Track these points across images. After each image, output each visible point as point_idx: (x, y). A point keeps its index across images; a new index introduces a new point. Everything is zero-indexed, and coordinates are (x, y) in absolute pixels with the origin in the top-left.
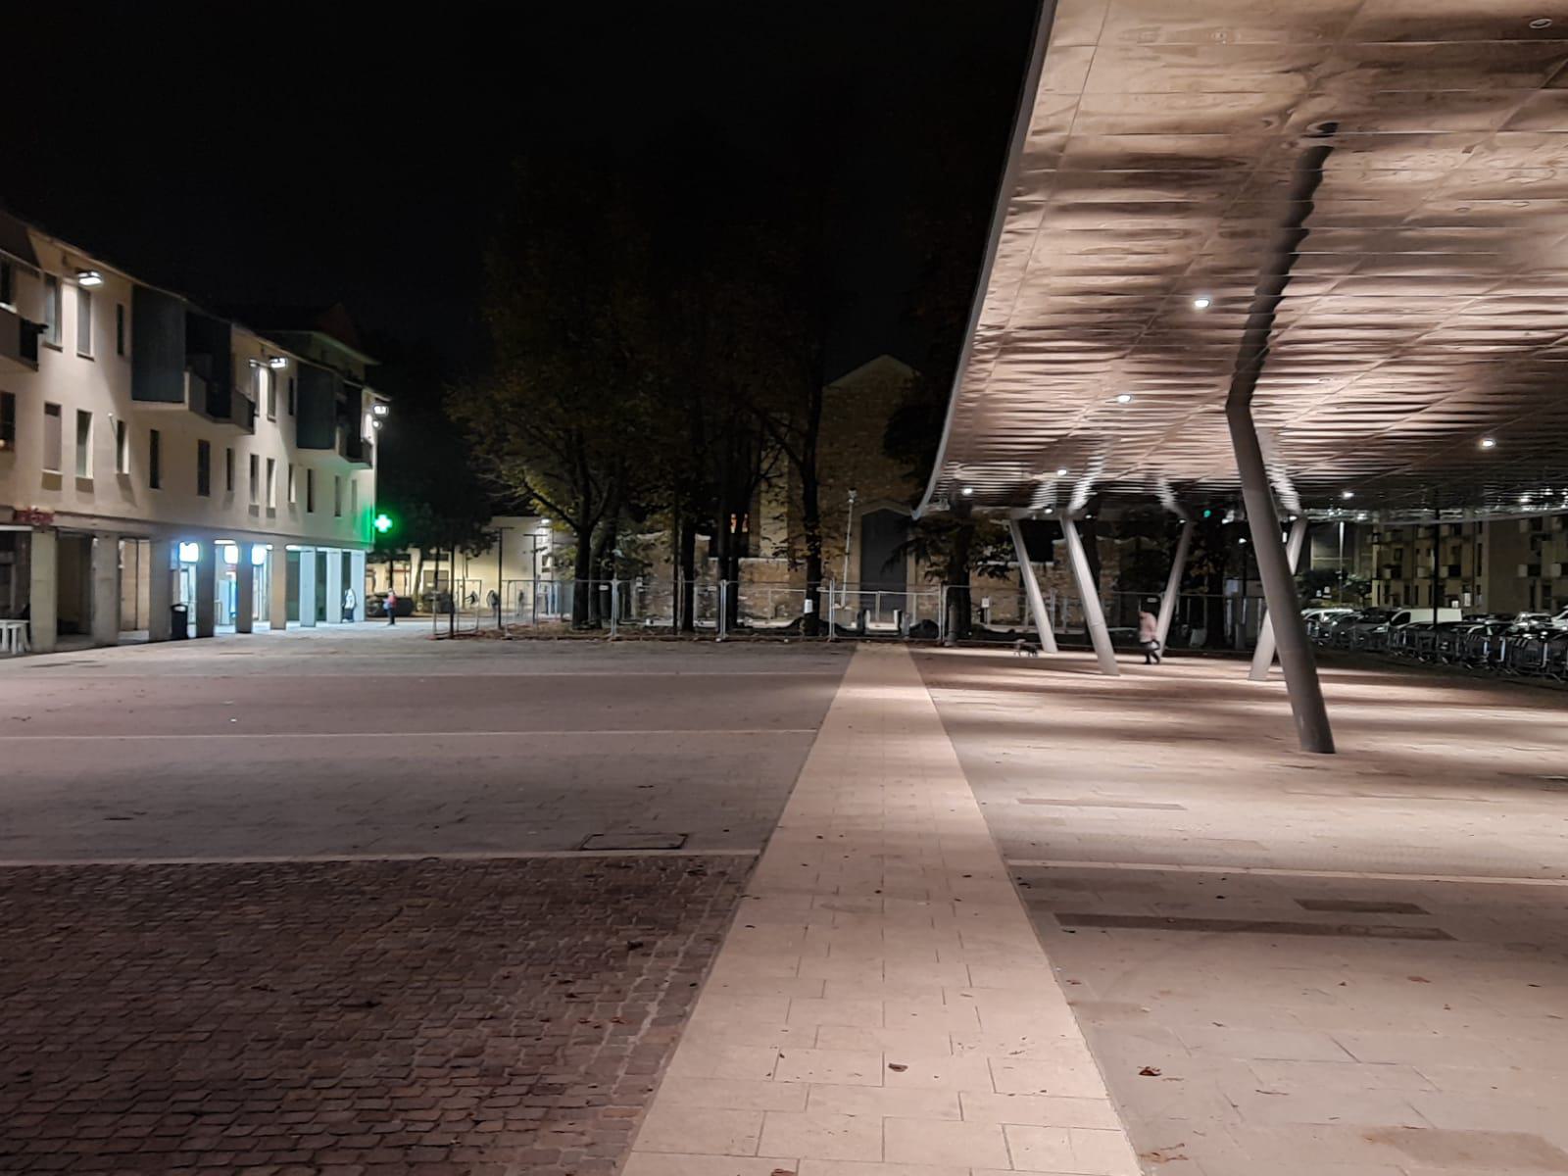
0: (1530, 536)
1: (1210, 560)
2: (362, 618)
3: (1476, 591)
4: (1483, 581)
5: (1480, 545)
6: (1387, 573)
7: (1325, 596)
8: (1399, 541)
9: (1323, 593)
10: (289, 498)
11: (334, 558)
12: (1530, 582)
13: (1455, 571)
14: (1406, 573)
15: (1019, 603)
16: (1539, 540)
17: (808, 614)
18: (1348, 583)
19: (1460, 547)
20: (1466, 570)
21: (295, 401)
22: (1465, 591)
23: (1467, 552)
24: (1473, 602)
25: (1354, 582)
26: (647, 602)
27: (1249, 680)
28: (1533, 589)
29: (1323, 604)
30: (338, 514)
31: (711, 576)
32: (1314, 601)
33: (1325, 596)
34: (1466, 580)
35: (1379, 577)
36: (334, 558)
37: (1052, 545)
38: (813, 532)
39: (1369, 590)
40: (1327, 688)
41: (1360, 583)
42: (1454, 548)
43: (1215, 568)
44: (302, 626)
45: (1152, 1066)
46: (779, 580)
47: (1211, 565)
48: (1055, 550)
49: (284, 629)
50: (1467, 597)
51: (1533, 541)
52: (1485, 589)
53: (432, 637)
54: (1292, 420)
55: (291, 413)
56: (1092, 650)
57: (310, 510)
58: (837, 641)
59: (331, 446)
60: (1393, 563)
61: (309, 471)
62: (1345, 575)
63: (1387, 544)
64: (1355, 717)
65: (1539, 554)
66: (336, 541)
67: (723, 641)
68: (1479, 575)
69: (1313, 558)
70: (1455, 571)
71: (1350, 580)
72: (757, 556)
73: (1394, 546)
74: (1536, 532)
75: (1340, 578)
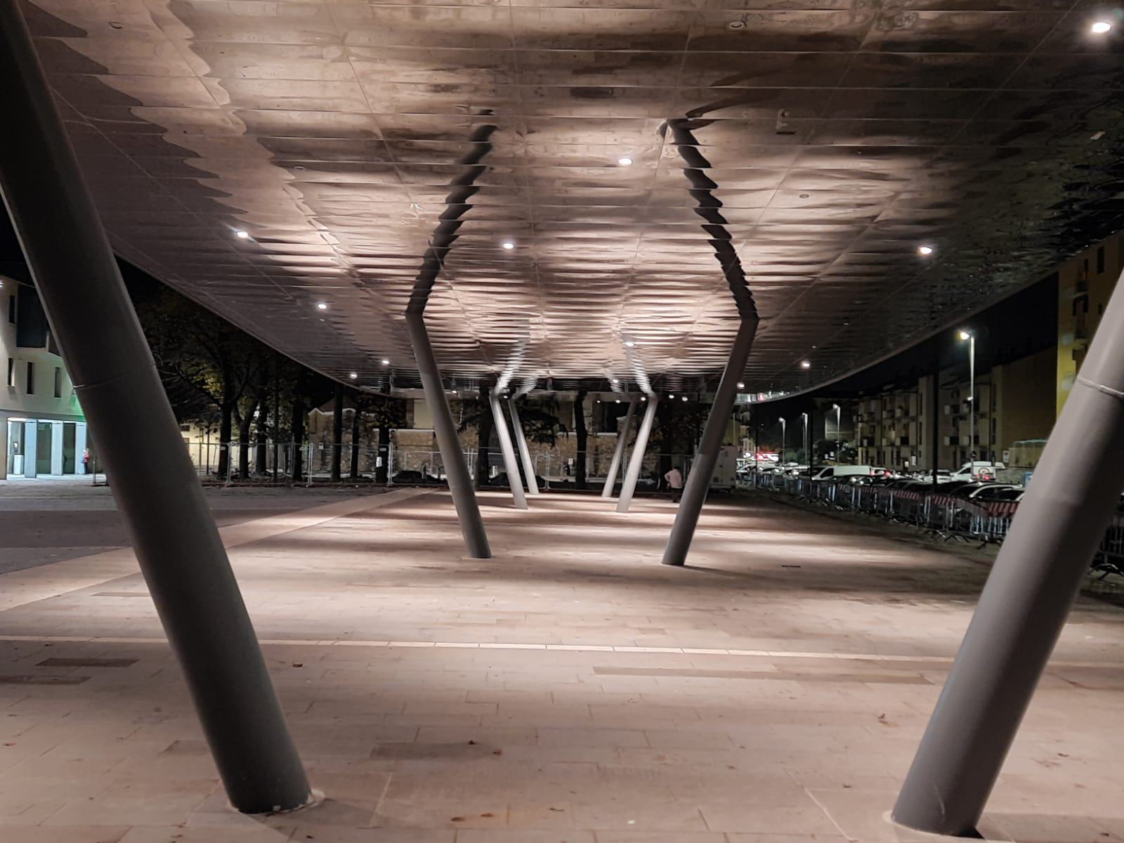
0: (951, 417)
1: (661, 430)
2: (83, 472)
3: (919, 455)
4: (922, 448)
5: (921, 423)
6: (865, 442)
7: (831, 459)
8: (873, 420)
9: (829, 456)
10: (10, 382)
11: (57, 429)
12: (952, 449)
13: (905, 441)
14: (877, 443)
15: (595, 462)
16: (958, 419)
17: (380, 468)
18: (844, 449)
19: (908, 424)
20: (912, 441)
21: (16, 310)
22: (912, 455)
23: (912, 426)
24: (917, 463)
25: (846, 448)
26: (327, 460)
27: (617, 511)
28: (955, 453)
29: (830, 464)
30: (57, 395)
31: (375, 442)
32: (824, 461)
33: (831, 459)
34: (912, 447)
35: (862, 445)
36: (57, 429)
37: (617, 421)
38: (379, 408)
39: (857, 454)
40: (485, 512)
41: (851, 449)
42: (905, 425)
43: (664, 436)
44: (26, 477)
45: (310, 835)
46: (425, 444)
47: (661, 433)
48: (618, 424)
49: (5, 479)
50: (914, 458)
51: (954, 420)
52: (924, 454)
53: (92, 484)
54: (319, 306)
55: (11, 320)
56: (509, 490)
57: (30, 391)
58: (393, 486)
59: (44, 346)
60: (870, 435)
61: (30, 365)
62: (841, 446)
63: (867, 422)
64: (608, 536)
65: (958, 430)
66: (55, 415)
67: (310, 487)
68: (921, 444)
69: (826, 432)
70: (905, 441)
71: (845, 447)
72: (412, 428)
73: (871, 424)
74: (956, 414)
75: (838, 446)
